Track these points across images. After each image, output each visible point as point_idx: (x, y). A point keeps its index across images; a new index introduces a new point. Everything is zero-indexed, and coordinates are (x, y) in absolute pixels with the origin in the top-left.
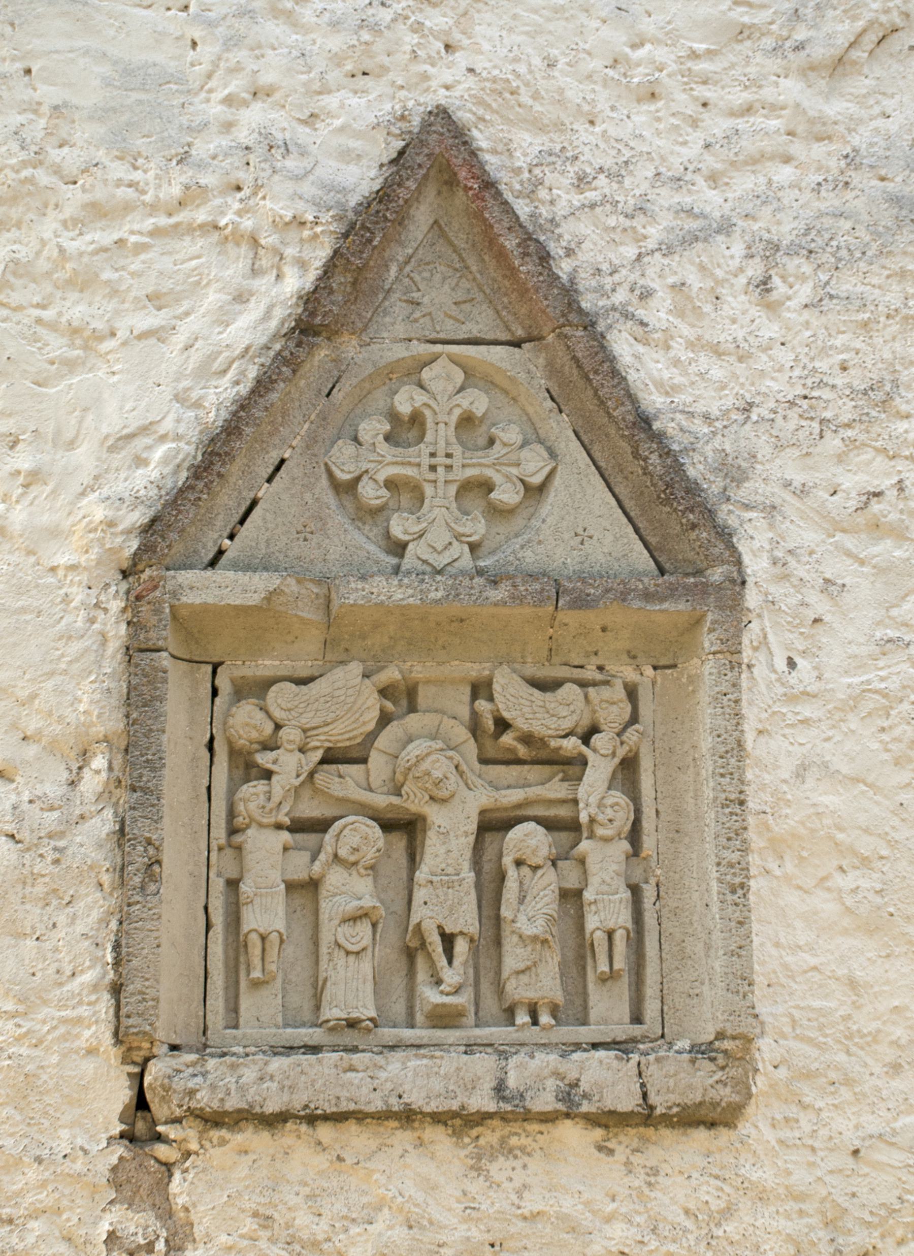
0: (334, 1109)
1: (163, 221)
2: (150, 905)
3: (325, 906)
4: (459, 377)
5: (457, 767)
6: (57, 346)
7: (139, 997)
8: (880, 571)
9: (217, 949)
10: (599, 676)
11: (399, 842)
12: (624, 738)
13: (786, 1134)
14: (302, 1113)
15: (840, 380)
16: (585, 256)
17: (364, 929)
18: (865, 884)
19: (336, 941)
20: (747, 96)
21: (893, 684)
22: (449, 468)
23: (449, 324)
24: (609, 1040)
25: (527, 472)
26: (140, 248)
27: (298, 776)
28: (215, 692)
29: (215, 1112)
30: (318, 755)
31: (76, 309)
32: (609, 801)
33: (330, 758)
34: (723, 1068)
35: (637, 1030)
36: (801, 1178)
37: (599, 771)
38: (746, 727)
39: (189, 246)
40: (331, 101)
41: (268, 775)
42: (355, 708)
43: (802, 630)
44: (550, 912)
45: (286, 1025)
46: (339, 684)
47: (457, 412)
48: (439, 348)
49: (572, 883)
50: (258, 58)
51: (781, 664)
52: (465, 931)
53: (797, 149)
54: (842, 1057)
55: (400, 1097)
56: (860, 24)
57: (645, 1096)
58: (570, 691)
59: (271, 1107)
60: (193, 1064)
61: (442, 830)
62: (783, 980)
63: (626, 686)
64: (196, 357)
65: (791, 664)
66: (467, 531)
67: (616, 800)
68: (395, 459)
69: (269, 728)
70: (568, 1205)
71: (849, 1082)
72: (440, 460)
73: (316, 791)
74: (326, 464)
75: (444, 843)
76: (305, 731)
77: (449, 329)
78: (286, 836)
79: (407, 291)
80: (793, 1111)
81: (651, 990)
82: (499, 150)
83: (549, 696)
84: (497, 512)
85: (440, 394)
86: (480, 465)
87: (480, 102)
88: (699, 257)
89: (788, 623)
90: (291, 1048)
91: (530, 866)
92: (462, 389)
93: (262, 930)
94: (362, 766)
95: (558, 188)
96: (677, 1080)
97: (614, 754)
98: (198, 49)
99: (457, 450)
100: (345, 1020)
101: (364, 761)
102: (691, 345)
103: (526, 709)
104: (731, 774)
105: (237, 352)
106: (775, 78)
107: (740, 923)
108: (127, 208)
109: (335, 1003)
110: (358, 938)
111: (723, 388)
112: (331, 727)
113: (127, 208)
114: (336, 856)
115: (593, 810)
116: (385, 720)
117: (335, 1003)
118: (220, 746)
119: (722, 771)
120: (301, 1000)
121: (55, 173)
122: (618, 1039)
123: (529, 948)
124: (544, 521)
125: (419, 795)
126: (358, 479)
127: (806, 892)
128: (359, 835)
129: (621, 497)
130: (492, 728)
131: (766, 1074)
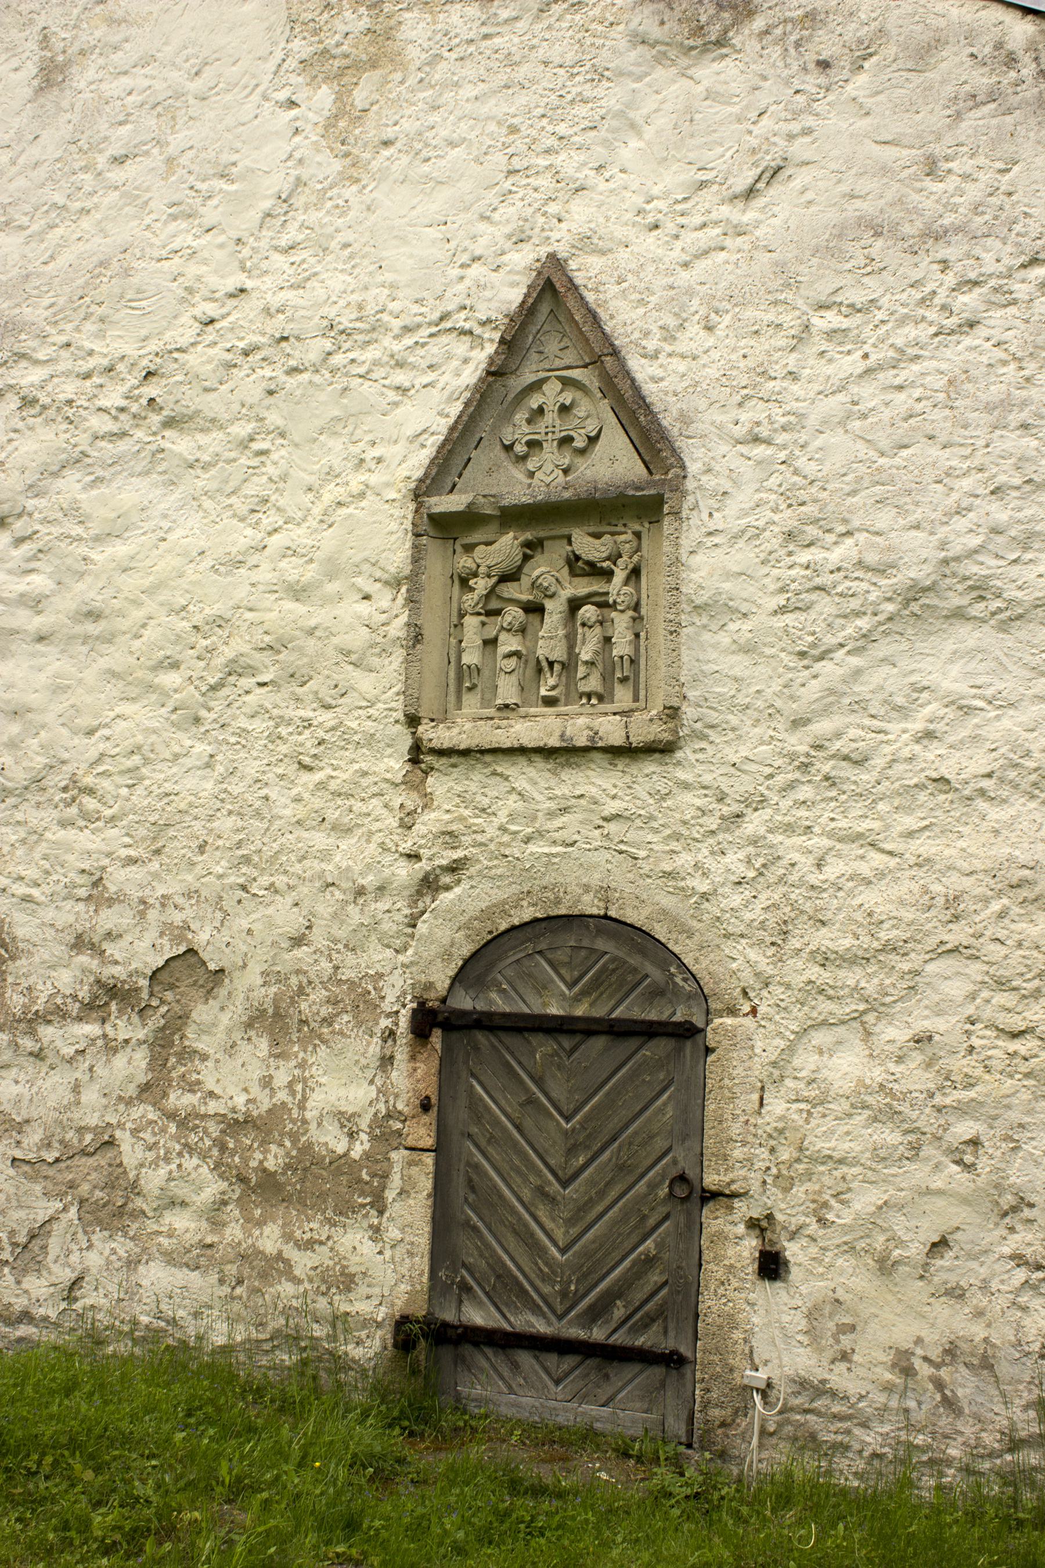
1: (434, 329)
6: (392, 396)
15: (742, 364)
16: (620, 318)
17: (513, 661)
20: (704, 219)
21: (761, 523)
26: (423, 345)
31: (401, 378)
33: (505, 578)
36: (707, 778)
37: (619, 576)
39: (444, 339)
40: (505, 258)
51: (705, 516)
53: (728, 242)
56: (759, 170)
64: (446, 393)
70: (594, 790)
77: (558, 363)
78: (483, 618)
85: (551, 395)
99: (558, 422)
108: (419, 326)
113: (419, 326)
116: (526, 558)
128: (513, 614)
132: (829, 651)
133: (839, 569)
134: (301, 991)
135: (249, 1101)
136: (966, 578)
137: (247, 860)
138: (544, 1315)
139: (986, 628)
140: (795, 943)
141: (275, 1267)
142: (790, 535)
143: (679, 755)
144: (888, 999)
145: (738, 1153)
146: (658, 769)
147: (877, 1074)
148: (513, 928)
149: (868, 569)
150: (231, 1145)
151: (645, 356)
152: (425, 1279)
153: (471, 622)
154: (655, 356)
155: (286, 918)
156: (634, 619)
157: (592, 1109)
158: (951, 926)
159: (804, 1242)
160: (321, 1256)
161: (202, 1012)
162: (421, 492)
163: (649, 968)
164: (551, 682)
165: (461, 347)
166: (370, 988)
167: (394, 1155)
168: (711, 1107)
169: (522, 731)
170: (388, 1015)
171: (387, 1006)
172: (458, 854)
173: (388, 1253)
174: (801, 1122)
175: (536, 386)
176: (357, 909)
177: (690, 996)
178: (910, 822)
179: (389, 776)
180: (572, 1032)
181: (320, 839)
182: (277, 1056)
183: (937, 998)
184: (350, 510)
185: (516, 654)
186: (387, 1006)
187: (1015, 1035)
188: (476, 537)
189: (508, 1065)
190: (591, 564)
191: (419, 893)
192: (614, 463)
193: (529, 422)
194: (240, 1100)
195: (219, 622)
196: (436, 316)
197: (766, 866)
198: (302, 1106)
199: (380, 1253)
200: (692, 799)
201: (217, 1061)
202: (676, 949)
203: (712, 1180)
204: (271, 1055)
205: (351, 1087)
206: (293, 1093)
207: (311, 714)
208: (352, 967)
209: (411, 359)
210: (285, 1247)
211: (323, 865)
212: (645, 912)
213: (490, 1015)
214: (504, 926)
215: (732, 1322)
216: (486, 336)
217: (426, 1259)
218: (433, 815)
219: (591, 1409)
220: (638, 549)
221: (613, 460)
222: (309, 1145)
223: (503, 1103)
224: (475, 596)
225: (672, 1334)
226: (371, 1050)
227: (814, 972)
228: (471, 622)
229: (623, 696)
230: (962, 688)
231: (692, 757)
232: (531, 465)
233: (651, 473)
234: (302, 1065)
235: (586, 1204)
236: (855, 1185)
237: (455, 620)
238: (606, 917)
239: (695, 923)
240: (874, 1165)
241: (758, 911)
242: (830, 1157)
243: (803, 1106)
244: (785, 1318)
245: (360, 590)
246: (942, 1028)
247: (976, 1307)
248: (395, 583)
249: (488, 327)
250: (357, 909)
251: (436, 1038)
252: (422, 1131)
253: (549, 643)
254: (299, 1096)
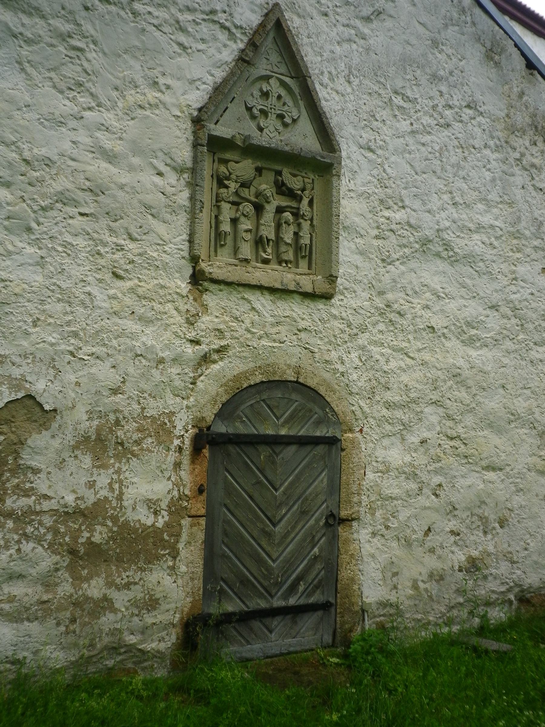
8: (369, 161)
9: (213, 235)
13: (341, 303)
18: (361, 242)
23: (275, 68)
26: (197, 24)
35: (310, 272)
36: (344, 315)
37: (305, 201)
48: (273, 74)
54: (353, 285)
59: (229, 280)
71: (355, 292)
77: (276, 69)
80: (342, 297)
83: (295, 179)
84: (285, 125)
102: (331, 89)
108: (195, 10)
113: (195, 10)
118: (215, 176)
128: (249, 208)
132: (394, 261)
133: (400, 223)
134: (117, 423)
135: (77, 498)
136: (443, 240)
137: (75, 335)
138: (265, 598)
139: (446, 263)
140: (378, 398)
141: (105, 604)
142: (381, 201)
144: (412, 424)
145: (355, 499)
147: (408, 459)
148: (250, 386)
149: (411, 226)
150: (62, 530)
152: (201, 592)
155: (106, 374)
157: (289, 484)
158: (434, 392)
159: (379, 537)
160: (136, 592)
161: (39, 440)
163: (317, 409)
166: (166, 421)
167: (183, 522)
168: (344, 478)
169: (260, 274)
170: (178, 438)
171: (177, 432)
172: (223, 343)
173: (180, 581)
174: (379, 482)
176: (158, 372)
177: (334, 423)
178: (419, 345)
179: (178, 290)
180: (280, 443)
181: (131, 326)
182: (98, 467)
183: (428, 423)
184: (148, 113)
186: (177, 432)
187: (452, 439)
188: (228, 156)
189: (246, 463)
191: (200, 364)
194: (70, 499)
195: (48, 162)
197: (367, 360)
198: (120, 498)
199: (175, 582)
200: (336, 324)
201: (49, 473)
202: (329, 400)
203: (344, 514)
204: (94, 466)
205: (152, 485)
206: (112, 490)
207: (123, 242)
208: (154, 408)
209: (190, 29)
210: (108, 592)
211: (134, 343)
212: (316, 381)
213: (238, 436)
214: (245, 385)
215: (353, 580)
217: (201, 581)
218: (208, 318)
219: (289, 641)
222: (127, 522)
223: (243, 484)
225: (326, 593)
226: (169, 459)
227: (385, 412)
230: (438, 287)
231: (338, 303)
234: (118, 472)
235: (285, 534)
236: (399, 509)
238: (297, 382)
239: (337, 387)
240: (407, 499)
241: (363, 382)
242: (391, 497)
243: (380, 474)
244: (373, 575)
245: (155, 168)
246: (430, 437)
247: (439, 555)
248: (180, 170)
249: (239, 31)
250: (158, 372)
251: (206, 452)
252: (199, 505)
254: (117, 492)
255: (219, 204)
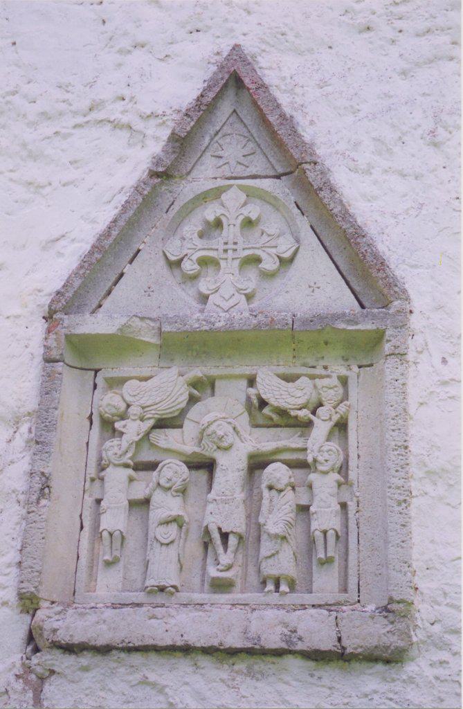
0: (140, 643)
1: (80, 120)
2: (40, 513)
3: (151, 514)
4: (243, 197)
5: (234, 429)
7: (30, 570)
9: (85, 543)
10: (323, 372)
11: (202, 476)
12: (337, 410)
14: (120, 646)
19: (155, 537)
20: (428, 24)
22: (235, 250)
23: (240, 168)
24: (323, 603)
25: (281, 251)
26: (66, 136)
27: (138, 435)
28: (95, 386)
29: (67, 644)
30: (152, 422)
32: (325, 448)
33: (161, 424)
34: (392, 623)
37: (321, 428)
38: (410, 401)
41: (122, 434)
42: (173, 394)
43: (452, 341)
44: (288, 519)
45: (123, 591)
46: (165, 380)
47: (241, 218)
48: (232, 182)
49: (304, 502)
50: (138, 27)
51: (437, 361)
52: (235, 531)
55: (182, 636)
57: (339, 639)
58: (303, 381)
60: (59, 613)
61: (224, 468)
62: (438, 566)
63: (339, 378)
65: (444, 361)
66: (243, 287)
67: (330, 447)
68: (203, 247)
69: (123, 406)
72: (231, 246)
73: (152, 445)
74: (163, 252)
75: (225, 476)
76: (143, 408)
77: (239, 170)
78: (130, 472)
79: (217, 150)
81: (352, 571)
82: (273, 67)
83: (290, 384)
85: (233, 206)
86: (253, 248)
87: (263, 41)
88: (392, 119)
89: (443, 336)
90: (124, 604)
91: (277, 490)
92: (245, 204)
93: (109, 530)
94: (180, 430)
95: (307, 86)
96: (365, 631)
97: (330, 419)
98: (106, 24)
99: (240, 240)
100: (157, 587)
101: (181, 427)
103: (275, 393)
104: (400, 429)
105: (117, 190)
106: (445, 12)
107: (404, 526)
109: (152, 576)
110: (168, 535)
111: (405, 196)
112: (159, 405)
114: (159, 484)
115: (315, 454)
116: (193, 400)
117: (152, 576)
119: (393, 428)
120: (135, 574)
121: (24, 97)
122: (329, 603)
123: (273, 542)
124: (290, 280)
125: (211, 446)
126: (182, 260)
127: (453, 507)
128: (173, 470)
129: (338, 264)
130: (257, 405)
131: (424, 629)
143: (410, 668)
146: (383, 687)
151: (355, 170)
153: (117, 477)
154: (368, 172)
156: (340, 485)
162: (57, 311)
164: (225, 559)
165: (116, 142)
175: (215, 194)
185: (176, 520)
190: (283, 413)
192: (316, 287)
193: (201, 235)
196: (86, 104)
216: (149, 132)
220: (346, 397)
221: (313, 287)
224: (125, 442)
228: (117, 477)
229: (326, 583)
231: (430, 673)
232: (204, 286)
233: (363, 307)
237: (92, 471)
249: (153, 122)
253: (225, 504)
255: (102, 474)
